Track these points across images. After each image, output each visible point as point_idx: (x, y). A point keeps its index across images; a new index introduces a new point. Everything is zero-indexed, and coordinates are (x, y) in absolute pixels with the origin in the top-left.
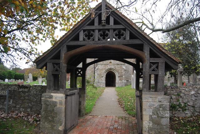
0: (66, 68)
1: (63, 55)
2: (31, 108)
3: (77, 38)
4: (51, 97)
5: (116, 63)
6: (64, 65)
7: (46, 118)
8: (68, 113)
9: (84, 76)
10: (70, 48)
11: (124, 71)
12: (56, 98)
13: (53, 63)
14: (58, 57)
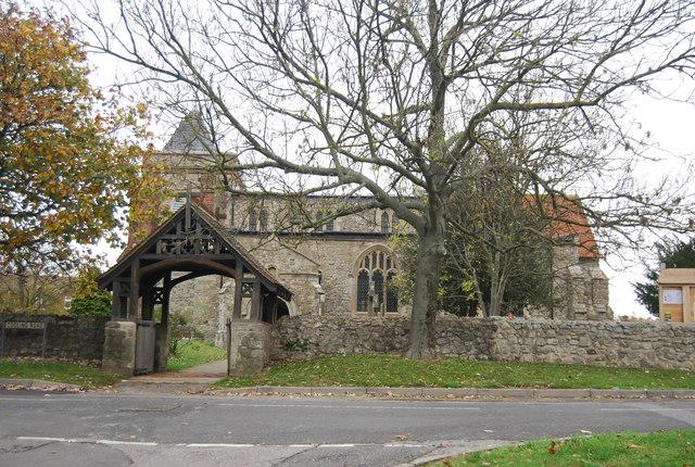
0: (138, 289)
1: (135, 272)
2: (79, 350)
3: (153, 250)
4: (118, 326)
5: (290, 271)
6: (135, 285)
7: (110, 352)
8: (140, 348)
9: (165, 303)
10: (144, 263)
11: (316, 298)
12: (124, 327)
13: (121, 283)
14: (127, 273)
